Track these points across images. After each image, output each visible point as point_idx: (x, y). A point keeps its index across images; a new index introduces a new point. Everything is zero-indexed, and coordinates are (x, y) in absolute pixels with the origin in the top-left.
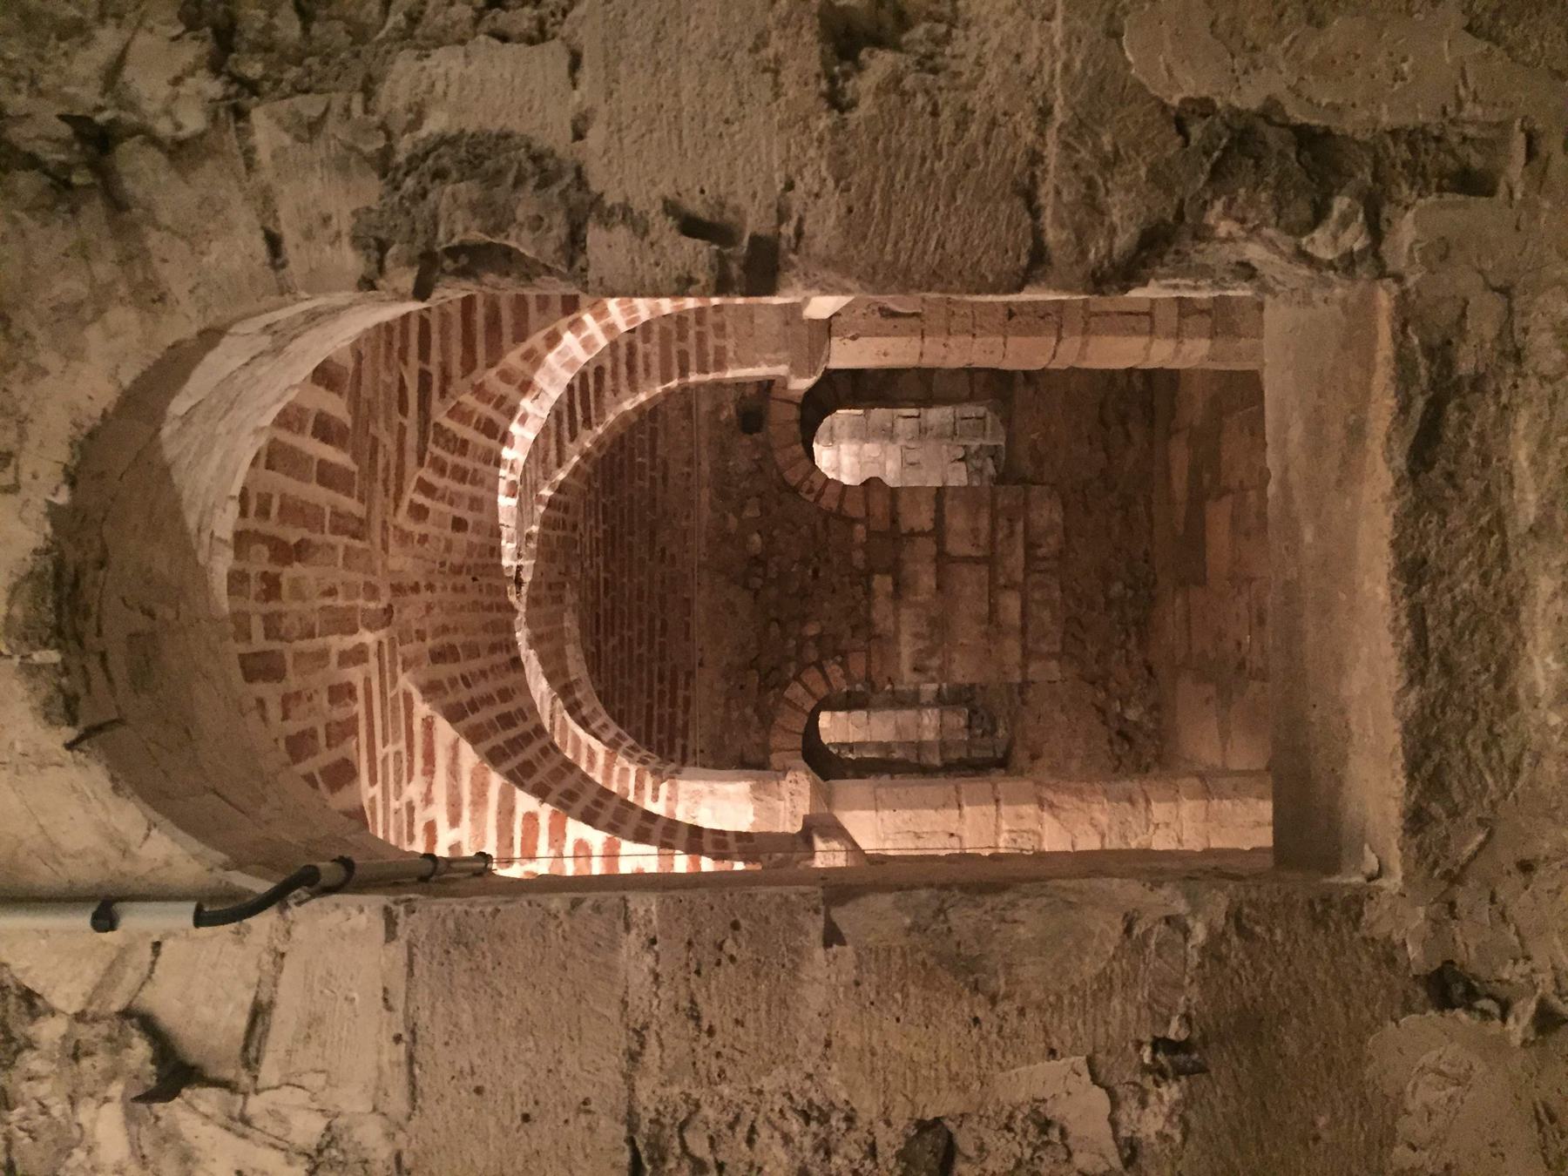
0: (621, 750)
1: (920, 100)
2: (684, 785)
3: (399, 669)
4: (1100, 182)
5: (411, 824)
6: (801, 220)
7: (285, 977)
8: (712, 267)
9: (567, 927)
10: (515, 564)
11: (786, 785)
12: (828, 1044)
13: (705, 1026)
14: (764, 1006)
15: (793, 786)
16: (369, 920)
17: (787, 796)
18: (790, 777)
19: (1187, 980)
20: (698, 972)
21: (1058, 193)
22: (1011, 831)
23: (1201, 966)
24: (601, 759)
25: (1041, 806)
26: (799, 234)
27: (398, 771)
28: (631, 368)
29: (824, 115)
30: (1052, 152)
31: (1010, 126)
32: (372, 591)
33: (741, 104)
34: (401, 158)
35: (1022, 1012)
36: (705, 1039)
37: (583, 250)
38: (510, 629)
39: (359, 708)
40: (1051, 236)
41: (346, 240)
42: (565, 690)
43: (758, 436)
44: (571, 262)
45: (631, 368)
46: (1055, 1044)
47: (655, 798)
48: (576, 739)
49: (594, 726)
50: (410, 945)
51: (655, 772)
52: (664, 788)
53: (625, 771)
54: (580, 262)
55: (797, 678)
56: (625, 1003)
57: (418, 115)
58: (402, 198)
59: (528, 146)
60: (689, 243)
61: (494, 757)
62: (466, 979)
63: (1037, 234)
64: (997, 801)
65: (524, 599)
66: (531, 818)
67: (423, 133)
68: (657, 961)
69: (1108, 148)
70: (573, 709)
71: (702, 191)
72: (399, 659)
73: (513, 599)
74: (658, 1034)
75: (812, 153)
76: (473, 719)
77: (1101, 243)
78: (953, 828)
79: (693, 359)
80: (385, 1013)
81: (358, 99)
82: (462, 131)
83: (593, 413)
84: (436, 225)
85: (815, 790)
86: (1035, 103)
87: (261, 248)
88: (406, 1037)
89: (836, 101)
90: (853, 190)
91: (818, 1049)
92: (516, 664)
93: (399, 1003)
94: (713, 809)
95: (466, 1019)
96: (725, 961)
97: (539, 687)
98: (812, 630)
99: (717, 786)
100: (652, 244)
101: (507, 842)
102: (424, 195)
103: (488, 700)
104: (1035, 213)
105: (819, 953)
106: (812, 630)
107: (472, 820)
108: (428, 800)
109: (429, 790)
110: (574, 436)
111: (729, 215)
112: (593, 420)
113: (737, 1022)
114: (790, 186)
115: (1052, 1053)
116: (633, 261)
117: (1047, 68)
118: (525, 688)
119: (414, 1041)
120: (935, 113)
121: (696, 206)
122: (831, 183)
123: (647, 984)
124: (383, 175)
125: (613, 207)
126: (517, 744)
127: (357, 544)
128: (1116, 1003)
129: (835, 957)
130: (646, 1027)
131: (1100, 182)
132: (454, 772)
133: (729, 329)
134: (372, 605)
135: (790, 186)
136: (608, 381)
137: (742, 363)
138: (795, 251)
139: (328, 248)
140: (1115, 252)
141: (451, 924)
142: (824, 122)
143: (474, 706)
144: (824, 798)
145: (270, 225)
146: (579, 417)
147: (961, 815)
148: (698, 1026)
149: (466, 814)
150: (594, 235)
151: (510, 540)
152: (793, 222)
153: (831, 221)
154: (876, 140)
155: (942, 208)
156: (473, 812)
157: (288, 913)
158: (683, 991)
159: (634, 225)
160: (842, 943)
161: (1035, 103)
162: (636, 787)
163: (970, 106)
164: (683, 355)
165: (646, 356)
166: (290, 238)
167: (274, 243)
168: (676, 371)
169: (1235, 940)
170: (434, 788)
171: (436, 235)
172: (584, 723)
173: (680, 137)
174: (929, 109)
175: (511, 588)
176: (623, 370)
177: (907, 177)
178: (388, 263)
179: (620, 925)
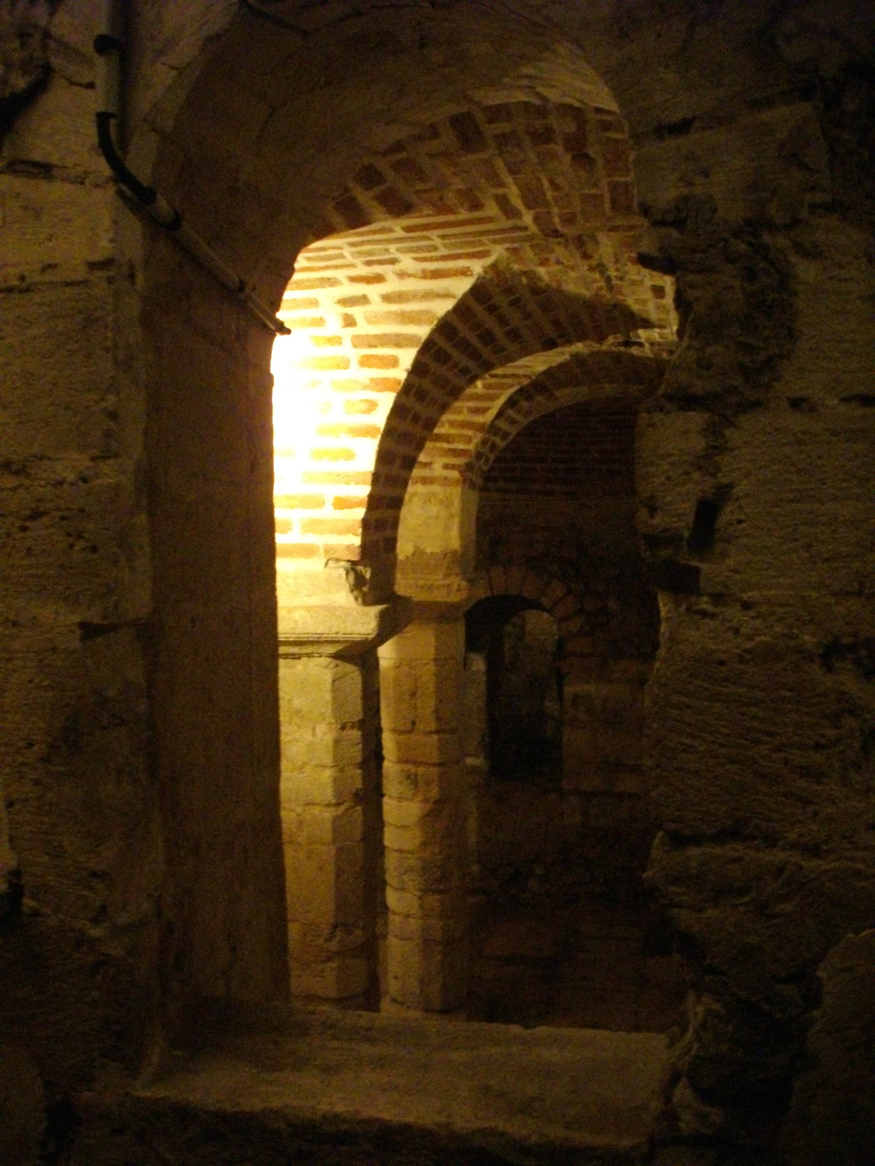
1: (831, 733)
2: (456, 493)
3: (507, 245)
4: (745, 900)
5: (381, 262)
6: (713, 616)
7: (68, 186)
8: (665, 530)
9: (93, 409)
10: (643, 340)
11: (456, 581)
12: (15, 624)
13: (28, 524)
14: (40, 572)
15: (455, 587)
16: (104, 247)
17: (447, 582)
18: (464, 584)
19: (61, 916)
20: (63, 518)
21: (734, 860)
22: (416, 775)
23: (72, 929)
24: (479, 419)
25: (437, 802)
26: (704, 614)
27: (369, 253)
29: (815, 640)
30: (778, 856)
31: (801, 818)
32: (569, 220)
33: (827, 560)
34: (766, 238)
35: (37, 782)
36: (18, 523)
37: (681, 408)
38: (582, 337)
39: (464, 215)
40: (694, 852)
41: (685, 191)
42: (538, 386)
44: (670, 398)
46: (17, 807)
47: (446, 467)
48: (492, 398)
49: (511, 412)
50: (85, 283)
51: (469, 467)
52: (455, 474)
53: (469, 440)
54: (668, 405)
55: (570, 591)
56: (42, 458)
57: (812, 253)
58: (726, 240)
59: (781, 356)
60: (688, 508)
61: (444, 327)
62: (61, 328)
63: (697, 840)
64: (441, 764)
65: (614, 349)
66: (394, 362)
67: (793, 259)
68: (72, 484)
69: (778, 908)
70: (524, 393)
71: (740, 522)
72: (516, 245)
73: (611, 339)
74: (21, 485)
75: (779, 629)
76: (479, 310)
77: (685, 898)
78: (421, 727)
80: (40, 266)
81: (826, 198)
82: (796, 294)
84: (701, 272)
85: (454, 606)
86: (825, 842)
87: (679, 115)
88: (24, 286)
89: (831, 653)
90: (741, 666)
91: (12, 616)
92: (549, 344)
93: (47, 277)
94: (437, 517)
95: (35, 331)
96: (70, 540)
97: (537, 363)
98: (613, 605)
99: (457, 520)
100: (687, 473)
101: (373, 342)
102: (731, 261)
103: (503, 321)
104: (720, 838)
105: (76, 619)
106: (613, 605)
107: (389, 313)
108: (402, 275)
109: (410, 276)
111: (719, 548)
113: (29, 549)
114: (746, 606)
115: (10, 804)
116: (670, 455)
117: (859, 854)
118: (526, 352)
119: (21, 292)
120: (818, 747)
121: (728, 514)
122: (749, 645)
123: (53, 476)
124: (747, 223)
125: (723, 436)
126: (464, 345)
127: (607, 205)
128: (46, 859)
129: (71, 631)
130: (28, 476)
131: (745, 900)
132: (428, 296)
134: (557, 220)
135: (746, 606)
138: (688, 609)
139: (676, 175)
140: (676, 910)
141: (99, 313)
142: (808, 639)
143: (492, 309)
144: (439, 614)
145: (698, 124)
147: (431, 732)
148: (26, 519)
149: (394, 307)
150: (697, 419)
151: (661, 336)
152: (710, 608)
153: (711, 645)
154: (791, 690)
155: (723, 750)
156: (396, 314)
157: (111, 184)
158: (49, 505)
159: (707, 457)
160: (83, 639)
161: (825, 842)
163: (826, 780)
166: (684, 142)
167: (682, 127)
169: (91, 959)
170: (411, 280)
171: (692, 272)
172: (511, 403)
173: (792, 501)
174: (823, 741)
175: (620, 338)
177: (754, 718)
178: (663, 231)
179: (96, 452)
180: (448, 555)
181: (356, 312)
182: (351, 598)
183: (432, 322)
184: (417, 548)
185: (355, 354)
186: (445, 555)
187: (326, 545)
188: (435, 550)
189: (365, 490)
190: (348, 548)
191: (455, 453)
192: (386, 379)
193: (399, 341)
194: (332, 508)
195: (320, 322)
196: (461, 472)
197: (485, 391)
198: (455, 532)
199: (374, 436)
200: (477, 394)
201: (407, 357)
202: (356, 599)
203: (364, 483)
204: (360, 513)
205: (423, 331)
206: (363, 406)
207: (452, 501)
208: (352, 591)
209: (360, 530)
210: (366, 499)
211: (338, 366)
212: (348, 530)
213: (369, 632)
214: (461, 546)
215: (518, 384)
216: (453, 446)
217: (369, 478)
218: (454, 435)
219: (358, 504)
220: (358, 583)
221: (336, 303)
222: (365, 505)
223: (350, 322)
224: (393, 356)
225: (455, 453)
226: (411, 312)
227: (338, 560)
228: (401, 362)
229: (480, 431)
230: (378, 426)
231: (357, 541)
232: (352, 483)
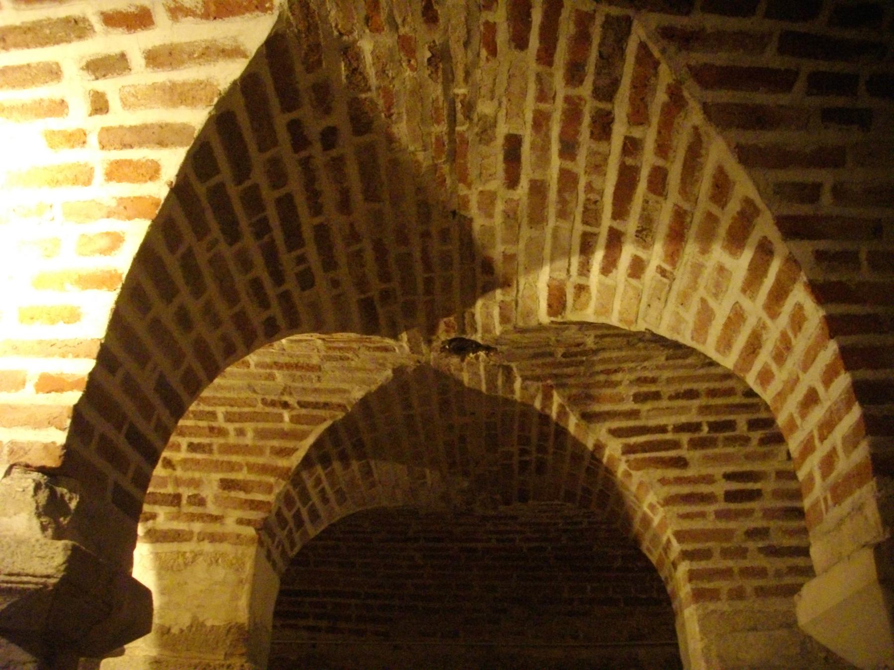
0: (290, 487)
24: (283, 463)
28: (688, 499)
43: (632, 398)
45: (688, 499)
47: (240, 522)
48: (303, 436)
52: (250, 531)
53: (269, 489)
66: (153, 171)
79: (703, 565)
83: (639, 456)
99: (247, 587)
101: (128, 139)
107: (154, 87)
110: (616, 433)
112: (632, 457)
133: (741, 605)
136: (672, 473)
137: (703, 620)
146: (633, 440)
149: (162, 76)
162: (252, 501)
164: (706, 554)
165: (702, 515)
168: (690, 547)
176: (685, 490)
180: (233, 630)
181: (110, 86)
182: (36, 523)
183: (212, 100)
184: (195, 618)
185: (98, 158)
186: (229, 631)
187: (12, 442)
188: (216, 623)
189: (85, 366)
190: (46, 447)
191: (254, 505)
192: (140, 198)
193: (160, 136)
194: (33, 390)
195: (60, 107)
196: (257, 530)
197: (293, 426)
198: (243, 602)
199: (111, 288)
200: (283, 429)
201: (172, 161)
202: (44, 528)
203: (87, 356)
204: (74, 397)
205: (196, 118)
206: (104, 243)
207: (244, 563)
208: (39, 515)
209: (68, 422)
210: (86, 379)
211: (75, 181)
212: (52, 422)
213: (50, 571)
214: (249, 618)
215: (331, 418)
216: (250, 497)
217: (96, 350)
218: (253, 481)
219: (73, 386)
220: (51, 510)
221: (82, 69)
222: (84, 386)
223: (100, 105)
224: (153, 161)
225: (254, 505)
226: (184, 84)
227: (28, 467)
228: (163, 171)
229: (283, 479)
230: (119, 272)
231: (60, 437)
232: (70, 355)
